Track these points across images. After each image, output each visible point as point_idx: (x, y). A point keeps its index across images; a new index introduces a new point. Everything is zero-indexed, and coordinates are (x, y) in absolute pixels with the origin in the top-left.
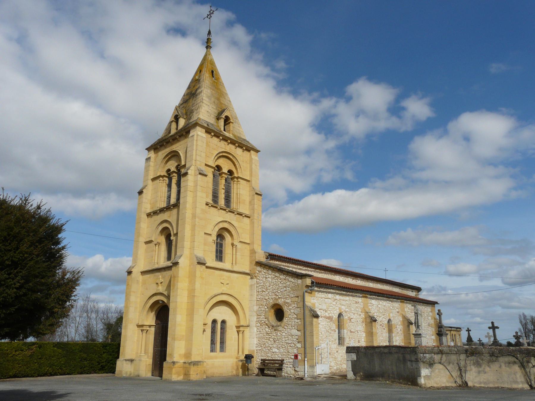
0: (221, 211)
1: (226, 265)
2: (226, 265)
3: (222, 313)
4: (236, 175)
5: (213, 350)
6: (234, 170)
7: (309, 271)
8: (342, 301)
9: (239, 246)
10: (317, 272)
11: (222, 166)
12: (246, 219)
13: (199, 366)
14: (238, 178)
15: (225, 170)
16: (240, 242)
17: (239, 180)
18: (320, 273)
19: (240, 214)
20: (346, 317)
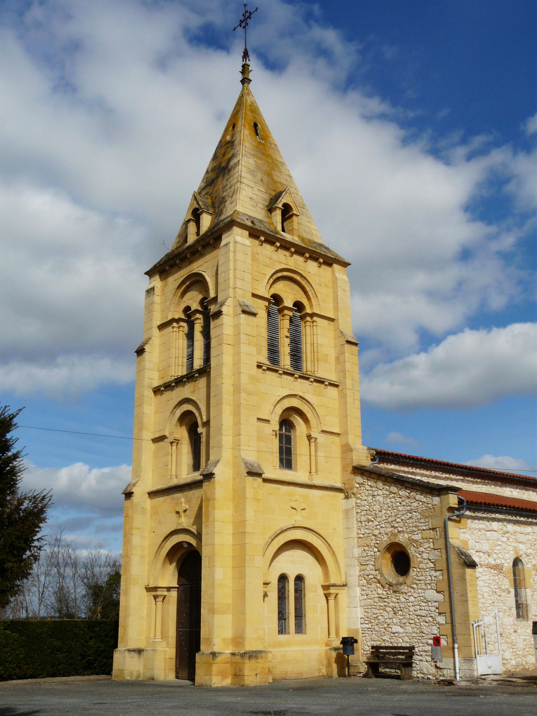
1: (299, 474)
2: (299, 474)
3: (295, 563)
4: (308, 310)
5: (282, 630)
6: (305, 301)
7: (452, 480)
8: (519, 536)
9: (322, 439)
10: (469, 482)
11: (283, 295)
12: (331, 389)
13: (259, 660)
14: (312, 315)
15: (288, 303)
16: (323, 431)
17: (315, 318)
18: (473, 483)
20: (529, 566)
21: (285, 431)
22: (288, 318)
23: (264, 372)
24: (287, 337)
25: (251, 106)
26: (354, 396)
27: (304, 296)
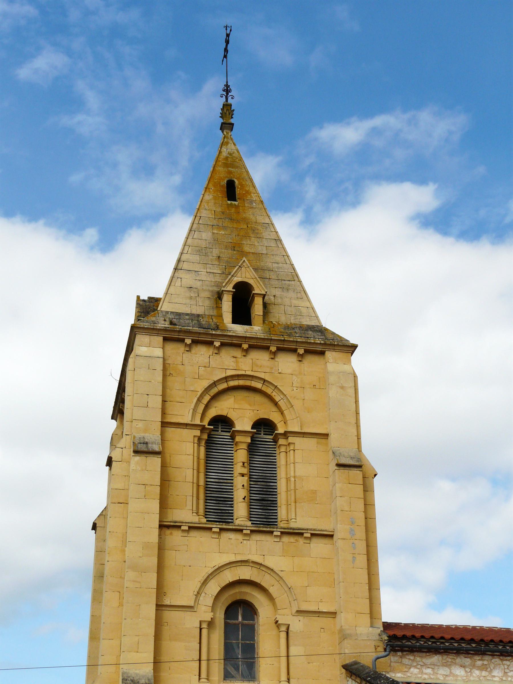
0: (194, 534)
6: (275, 417)
9: (297, 625)
11: (232, 415)
14: (286, 435)
15: (244, 423)
16: (300, 612)
19: (298, 533)
21: (244, 618)
22: (245, 446)
23: (186, 534)
24: (243, 475)
25: (227, 158)
26: (354, 548)
27: (274, 409)
